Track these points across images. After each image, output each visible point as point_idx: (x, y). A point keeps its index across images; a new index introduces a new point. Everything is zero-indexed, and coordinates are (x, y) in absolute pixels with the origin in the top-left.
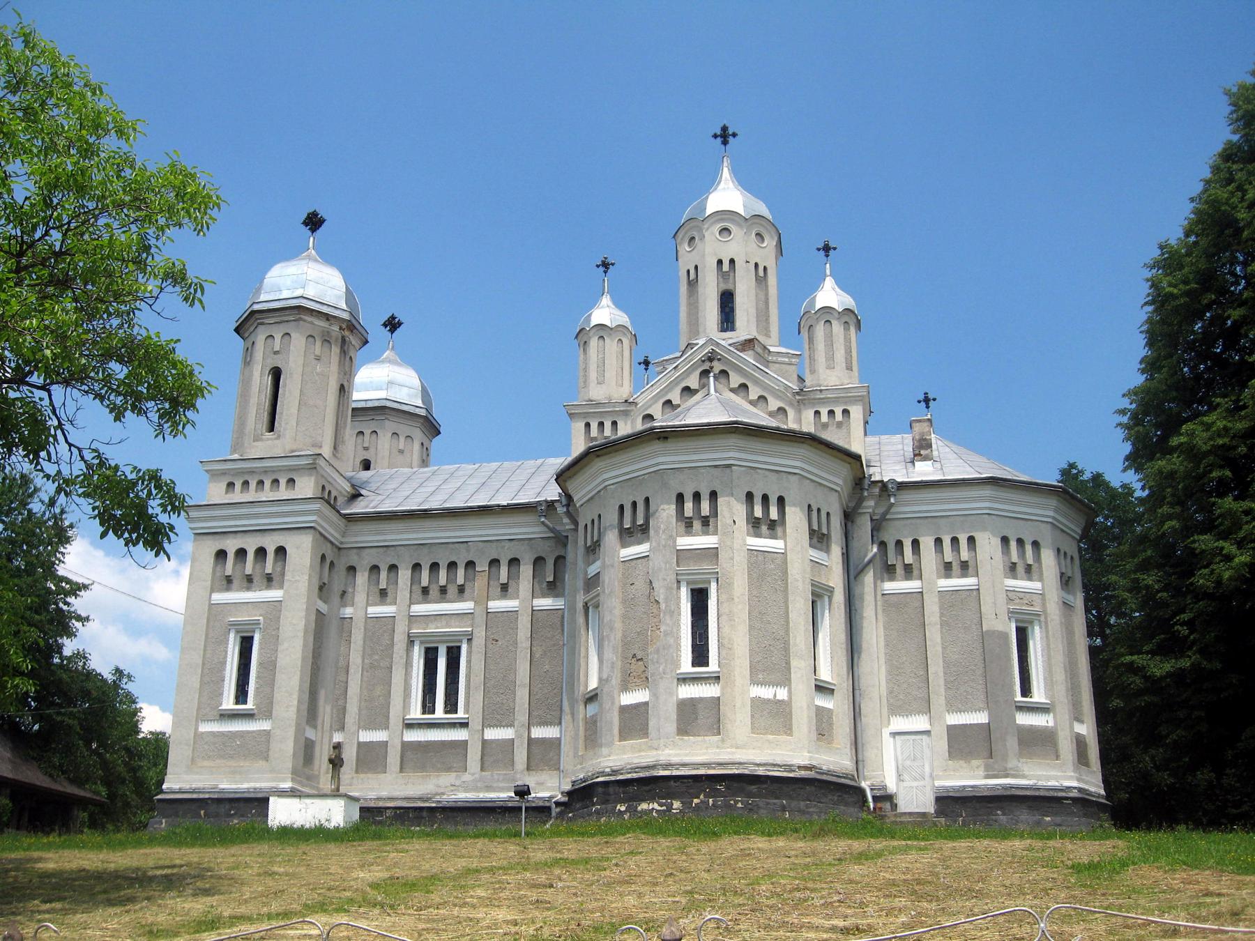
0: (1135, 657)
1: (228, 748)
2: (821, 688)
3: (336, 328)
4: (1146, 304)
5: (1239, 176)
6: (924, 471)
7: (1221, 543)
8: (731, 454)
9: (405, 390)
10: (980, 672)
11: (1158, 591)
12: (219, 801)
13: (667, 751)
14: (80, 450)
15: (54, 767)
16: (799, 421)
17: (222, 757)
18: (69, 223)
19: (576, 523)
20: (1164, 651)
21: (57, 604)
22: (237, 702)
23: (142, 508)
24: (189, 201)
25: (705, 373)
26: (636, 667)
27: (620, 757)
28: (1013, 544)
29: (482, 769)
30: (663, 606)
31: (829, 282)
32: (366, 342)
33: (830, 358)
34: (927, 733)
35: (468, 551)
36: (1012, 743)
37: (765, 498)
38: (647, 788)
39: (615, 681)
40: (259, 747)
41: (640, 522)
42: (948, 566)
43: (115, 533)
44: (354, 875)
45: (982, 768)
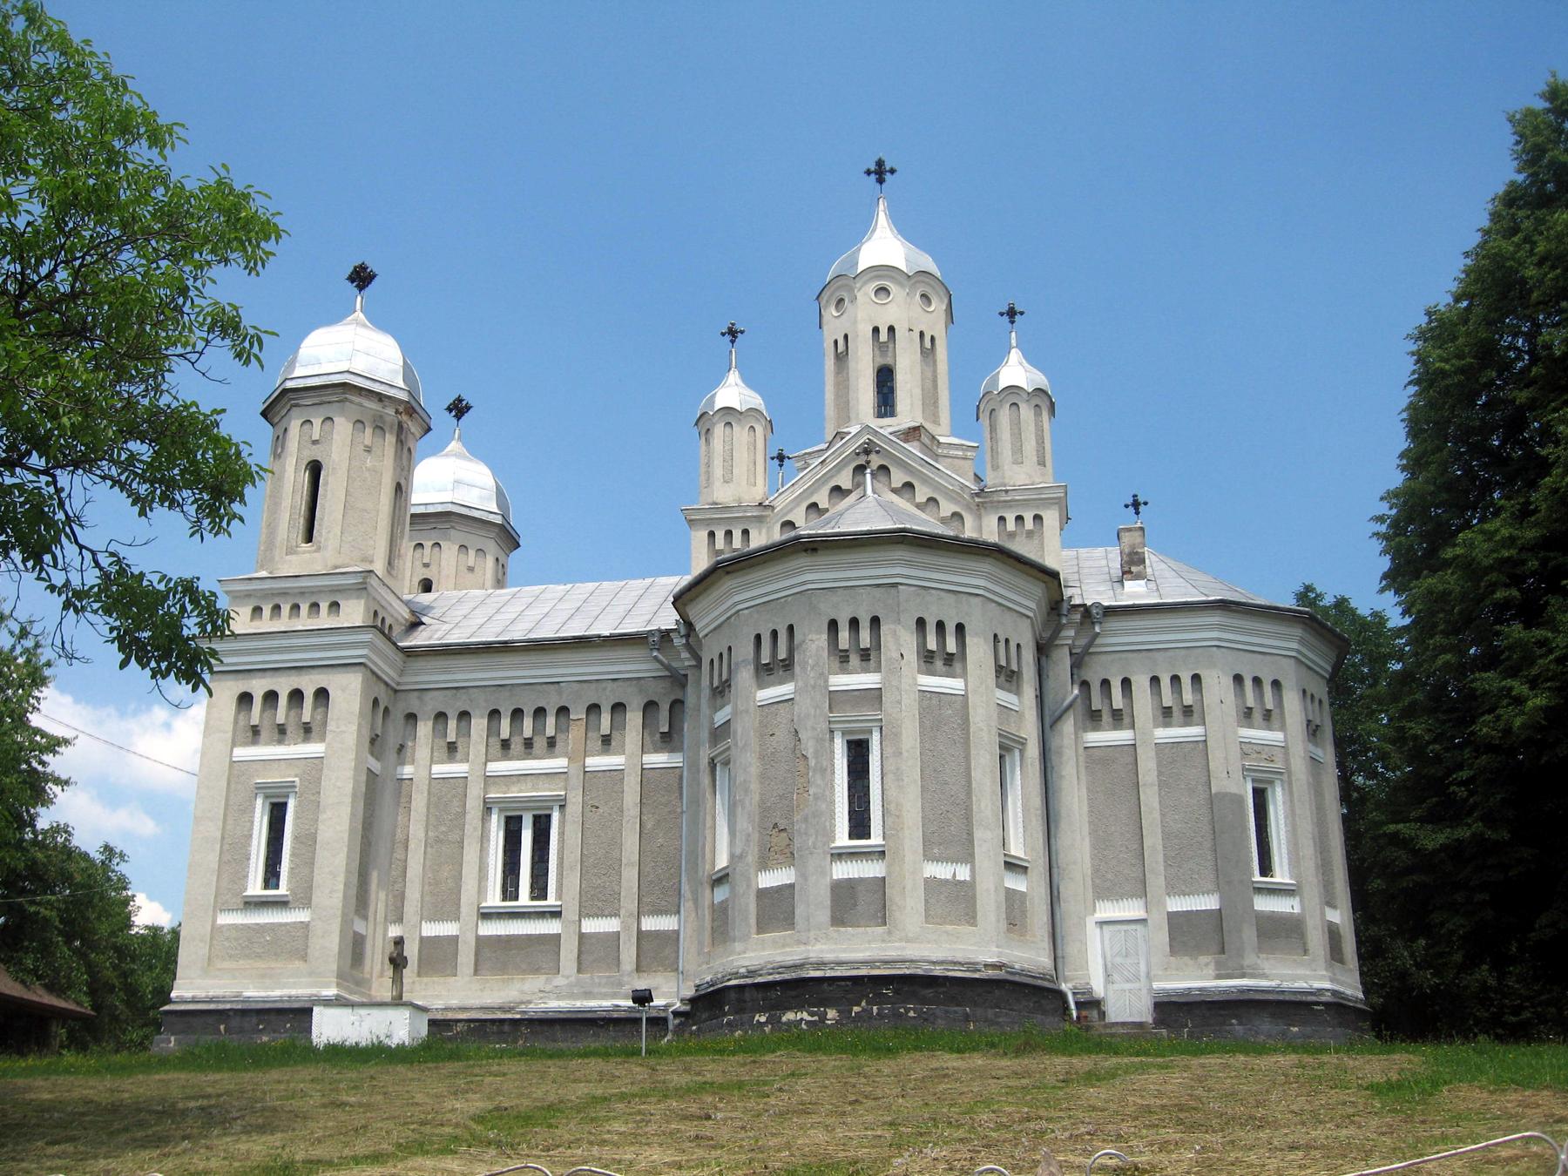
0: (1401, 826)
1: (253, 944)
2: (1012, 866)
3: (391, 411)
4: (1410, 383)
5: (1526, 224)
6: (1135, 592)
7: (1508, 682)
8: (898, 570)
9: (476, 492)
10: (1208, 844)
11: (1429, 743)
12: (244, 1013)
13: (818, 946)
14: (94, 553)
15: (29, 972)
16: (980, 529)
17: (247, 957)
18: (83, 258)
19: (699, 660)
20: (1434, 818)
21: (29, 764)
22: (266, 887)
23: (175, 624)
24: (238, 228)
25: (860, 469)
26: (779, 836)
27: (759, 954)
28: (1248, 684)
29: (579, 971)
30: (812, 763)
31: (1015, 355)
32: (429, 429)
33: (1018, 450)
34: (1143, 921)
35: (560, 693)
36: (1249, 934)
37: (940, 626)
38: (793, 993)
39: (752, 857)
40: (295, 944)
41: (782, 654)
42: (1167, 712)
43: (139, 661)
44: (448, 1105)
45: (1212, 966)
